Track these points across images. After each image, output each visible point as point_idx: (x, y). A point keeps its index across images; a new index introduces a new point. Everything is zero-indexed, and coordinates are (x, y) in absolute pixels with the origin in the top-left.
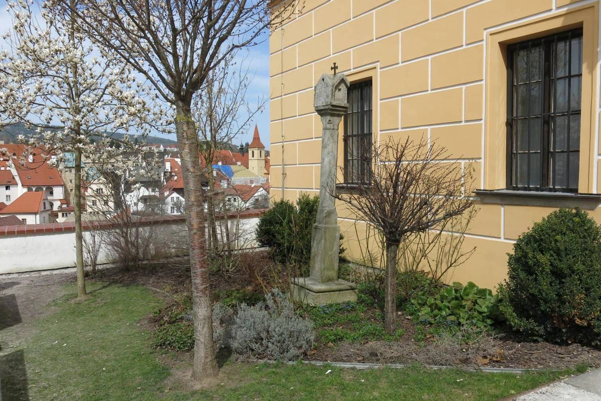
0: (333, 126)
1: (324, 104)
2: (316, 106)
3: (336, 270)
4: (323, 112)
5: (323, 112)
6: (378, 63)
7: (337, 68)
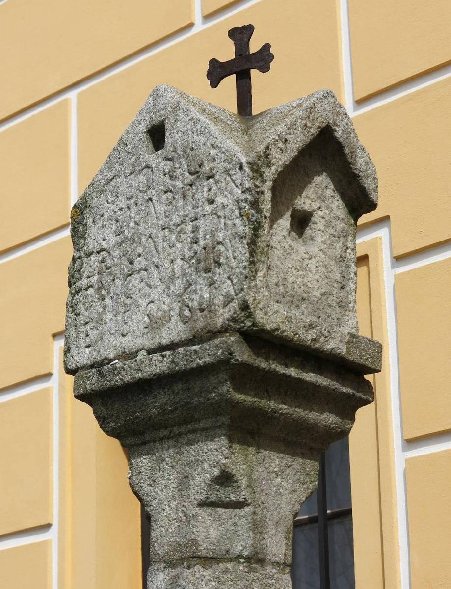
0: (257, 527)
1: (174, 331)
2: (82, 357)
4: (158, 402)
5: (158, 402)
6: (382, 233)
7: (264, 59)
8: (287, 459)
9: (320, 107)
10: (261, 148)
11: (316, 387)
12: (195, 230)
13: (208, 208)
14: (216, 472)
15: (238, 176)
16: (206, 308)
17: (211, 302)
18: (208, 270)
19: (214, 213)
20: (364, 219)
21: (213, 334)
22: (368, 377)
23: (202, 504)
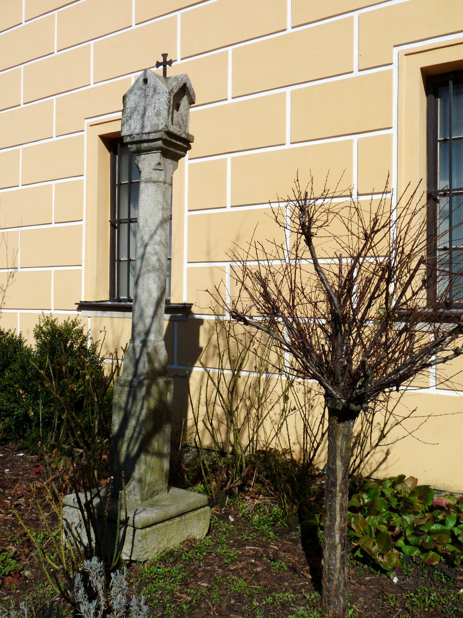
3: (165, 470)
7: (170, 63)
8: (172, 161)
9: (184, 79)
10: (171, 88)
11: (179, 145)
12: (155, 106)
13: (158, 101)
14: (157, 162)
15: (166, 94)
16: (157, 125)
17: (158, 124)
18: (157, 116)
19: (160, 103)
20: (192, 105)
21: (159, 131)
22: (190, 143)
23: (154, 169)
